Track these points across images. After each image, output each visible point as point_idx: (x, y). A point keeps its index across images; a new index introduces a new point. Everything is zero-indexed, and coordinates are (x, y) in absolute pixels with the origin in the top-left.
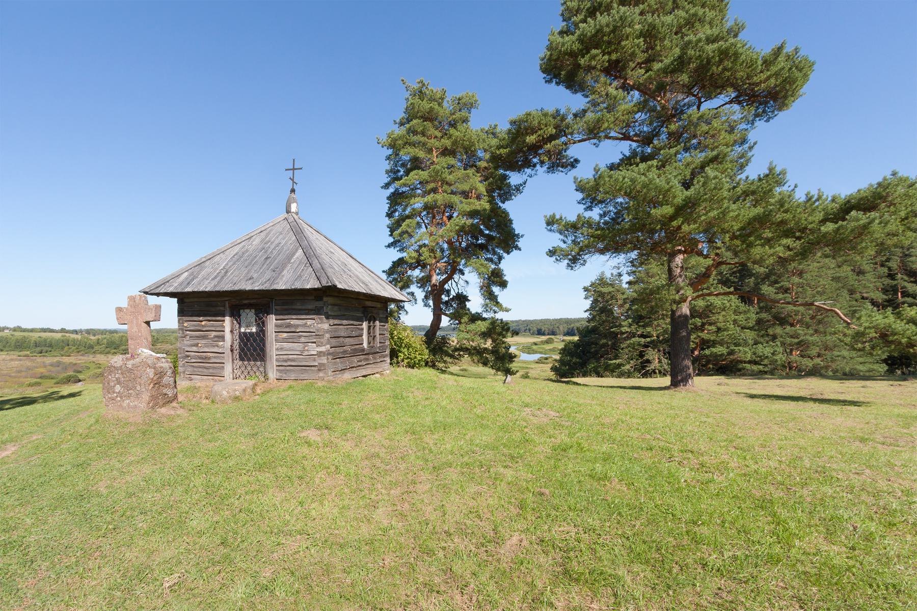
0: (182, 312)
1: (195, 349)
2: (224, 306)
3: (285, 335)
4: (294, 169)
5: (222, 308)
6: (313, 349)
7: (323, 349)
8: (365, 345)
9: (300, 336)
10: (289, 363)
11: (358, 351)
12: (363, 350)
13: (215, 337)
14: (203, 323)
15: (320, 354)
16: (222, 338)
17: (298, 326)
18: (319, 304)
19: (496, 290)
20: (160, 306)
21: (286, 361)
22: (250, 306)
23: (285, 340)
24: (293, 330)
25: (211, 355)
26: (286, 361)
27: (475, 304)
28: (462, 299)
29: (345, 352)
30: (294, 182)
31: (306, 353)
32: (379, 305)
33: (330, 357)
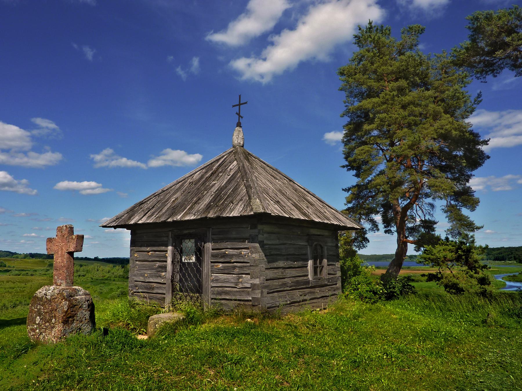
0: (134, 243)
1: (142, 279)
2: (168, 237)
3: (220, 265)
4: (240, 105)
5: (165, 239)
6: (247, 281)
7: (257, 281)
8: (310, 277)
9: (234, 267)
10: (223, 297)
11: (302, 284)
12: (308, 282)
13: (160, 267)
14: (150, 253)
15: (253, 287)
16: (164, 268)
17: (232, 256)
18: (254, 232)
19: (465, 211)
20: (82, 237)
21: (220, 293)
22: (189, 236)
23: (222, 271)
24: (228, 260)
25: (155, 285)
26: (220, 293)
27: (442, 228)
28: (429, 225)
29: (284, 284)
30: (240, 116)
31: (240, 286)
32: (326, 233)
33: (265, 291)
